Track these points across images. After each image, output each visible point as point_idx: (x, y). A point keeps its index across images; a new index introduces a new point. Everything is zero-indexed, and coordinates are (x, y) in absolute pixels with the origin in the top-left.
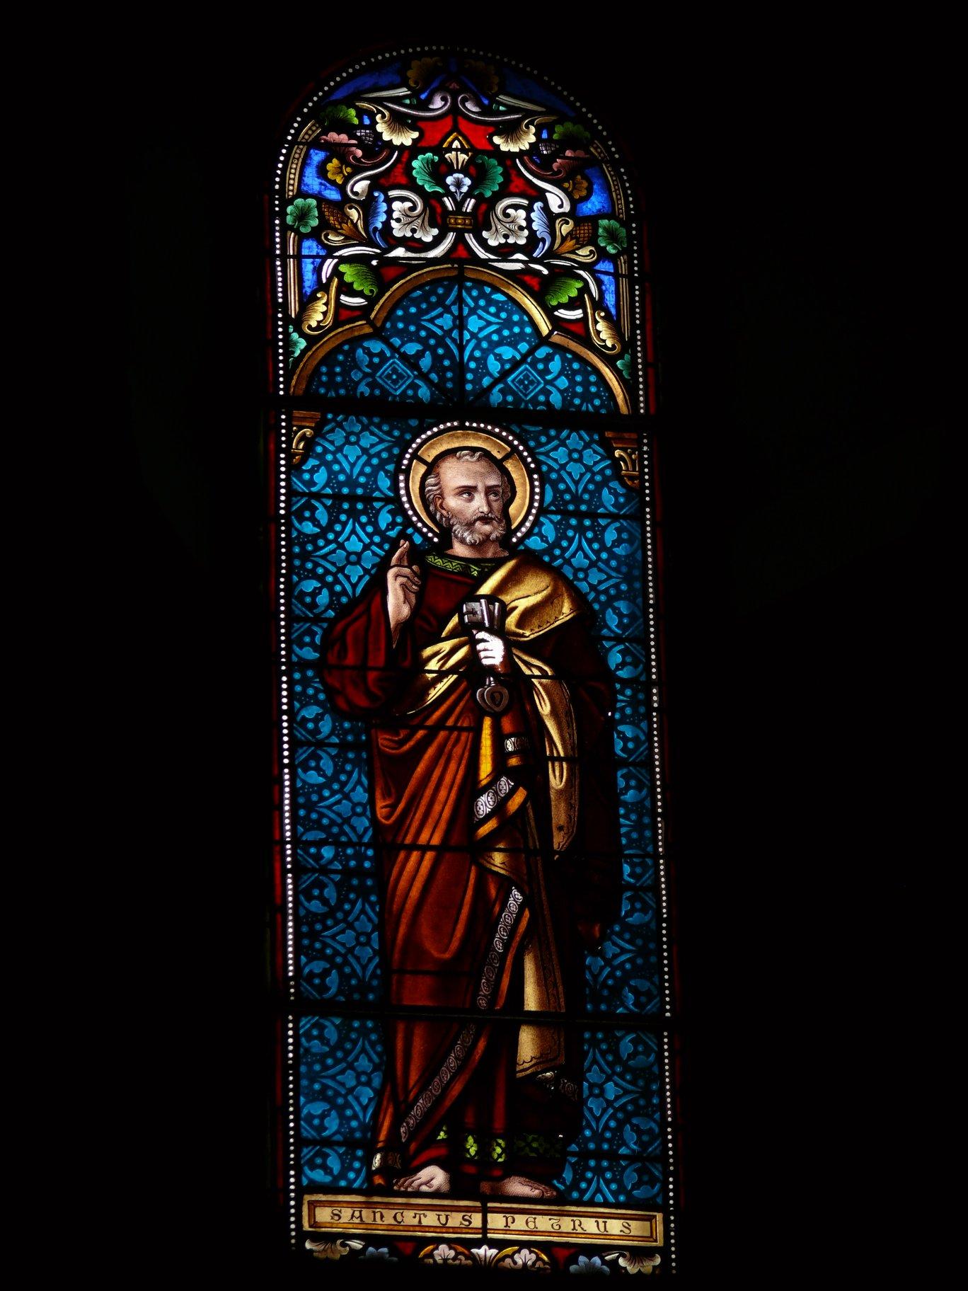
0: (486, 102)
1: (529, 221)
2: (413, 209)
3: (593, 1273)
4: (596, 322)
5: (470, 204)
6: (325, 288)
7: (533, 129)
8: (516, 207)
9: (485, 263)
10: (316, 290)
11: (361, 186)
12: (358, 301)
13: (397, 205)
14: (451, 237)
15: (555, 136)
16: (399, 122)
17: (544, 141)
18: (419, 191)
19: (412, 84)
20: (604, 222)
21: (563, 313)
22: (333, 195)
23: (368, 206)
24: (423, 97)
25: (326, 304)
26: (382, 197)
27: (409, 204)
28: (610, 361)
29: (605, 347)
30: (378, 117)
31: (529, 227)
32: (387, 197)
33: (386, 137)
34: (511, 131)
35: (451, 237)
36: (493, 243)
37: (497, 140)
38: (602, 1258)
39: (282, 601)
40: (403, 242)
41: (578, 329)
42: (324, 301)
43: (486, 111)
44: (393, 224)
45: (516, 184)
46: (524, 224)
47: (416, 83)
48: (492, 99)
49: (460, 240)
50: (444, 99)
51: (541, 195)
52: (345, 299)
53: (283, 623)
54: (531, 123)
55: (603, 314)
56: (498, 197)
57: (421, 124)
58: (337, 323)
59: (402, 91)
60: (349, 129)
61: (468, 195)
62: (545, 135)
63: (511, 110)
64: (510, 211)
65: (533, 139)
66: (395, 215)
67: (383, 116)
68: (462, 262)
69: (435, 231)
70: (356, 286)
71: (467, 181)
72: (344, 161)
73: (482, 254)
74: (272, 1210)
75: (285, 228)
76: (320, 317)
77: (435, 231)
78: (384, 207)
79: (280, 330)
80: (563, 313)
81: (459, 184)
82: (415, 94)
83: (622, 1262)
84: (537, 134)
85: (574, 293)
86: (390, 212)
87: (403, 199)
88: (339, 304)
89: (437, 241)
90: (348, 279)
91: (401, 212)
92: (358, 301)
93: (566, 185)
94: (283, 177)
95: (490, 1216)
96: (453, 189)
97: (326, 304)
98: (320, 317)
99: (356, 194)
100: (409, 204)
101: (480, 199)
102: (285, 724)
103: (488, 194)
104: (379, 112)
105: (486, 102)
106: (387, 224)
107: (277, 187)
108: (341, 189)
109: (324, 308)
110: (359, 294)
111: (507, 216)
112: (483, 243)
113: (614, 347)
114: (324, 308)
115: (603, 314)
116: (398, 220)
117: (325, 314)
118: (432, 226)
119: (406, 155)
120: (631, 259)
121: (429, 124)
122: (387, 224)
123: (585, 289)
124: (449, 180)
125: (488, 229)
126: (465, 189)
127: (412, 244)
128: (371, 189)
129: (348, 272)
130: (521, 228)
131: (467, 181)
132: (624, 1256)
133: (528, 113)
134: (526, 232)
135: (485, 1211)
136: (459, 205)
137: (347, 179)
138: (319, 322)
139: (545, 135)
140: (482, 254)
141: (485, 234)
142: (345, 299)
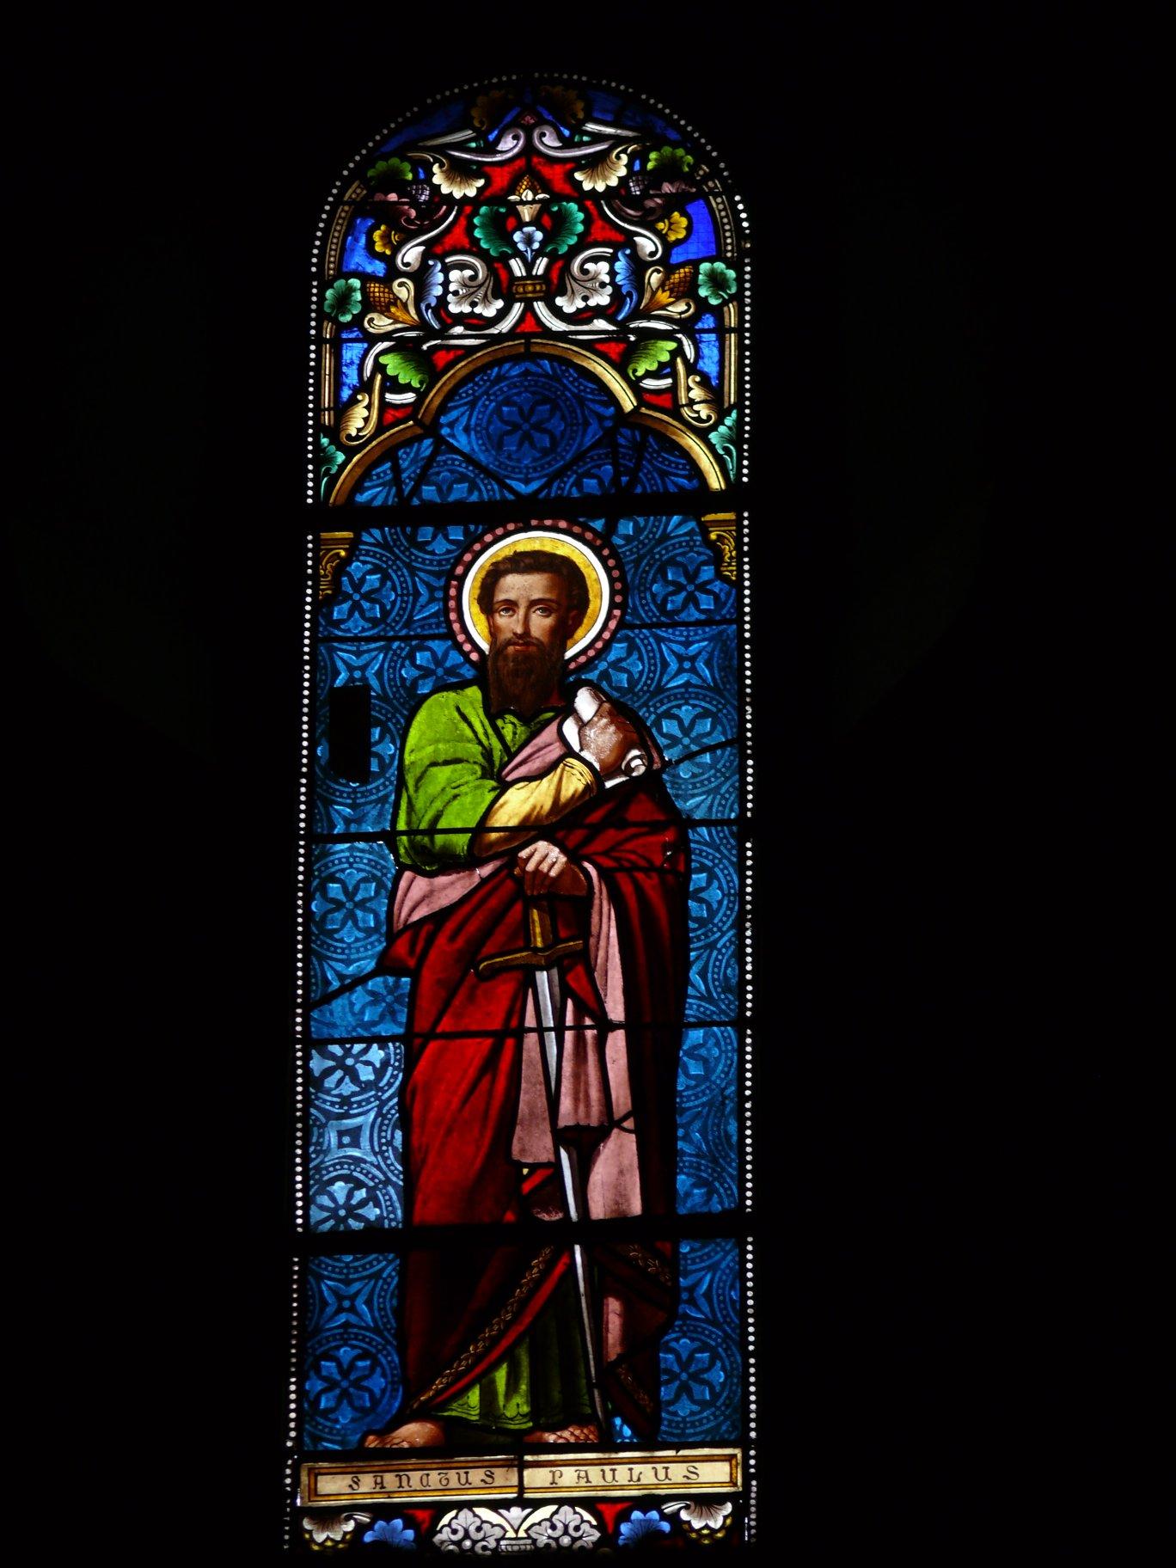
0: (567, 133)
1: (612, 273)
2: (473, 278)
3: (650, 1535)
4: (689, 389)
5: (541, 266)
6: (365, 386)
7: (624, 158)
8: (595, 259)
9: (562, 336)
10: (364, 391)
11: (411, 254)
12: (409, 397)
13: (455, 275)
14: (517, 308)
15: (650, 166)
16: (460, 171)
17: (636, 174)
18: (483, 255)
19: (477, 124)
20: (705, 267)
21: (650, 384)
22: (378, 268)
23: (420, 277)
24: (491, 137)
25: (368, 407)
26: (439, 266)
27: (468, 273)
28: (703, 434)
29: (699, 419)
30: (436, 168)
31: (613, 283)
32: (444, 264)
33: (445, 190)
34: (595, 164)
35: (517, 308)
36: (569, 309)
37: (578, 176)
38: (661, 1512)
39: (300, 965)
40: (460, 319)
41: (665, 401)
42: (366, 402)
43: (567, 144)
44: (450, 298)
45: (598, 232)
46: (607, 279)
47: (482, 123)
48: (577, 129)
49: (529, 310)
50: (516, 137)
51: (628, 240)
52: (391, 397)
53: (305, 761)
54: (624, 152)
55: (698, 379)
56: (575, 251)
57: (487, 169)
58: (381, 428)
59: (469, 133)
60: (402, 187)
61: (538, 253)
62: (637, 167)
63: (597, 138)
64: (587, 266)
65: (623, 172)
66: (452, 288)
67: (441, 166)
68: (528, 336)
69: (500, 304)
70: (402, 380)
71: (539, 236)
72: (393, 225)
73: (557, 325)
74: (275, 1512)
75: (322, 317)
76: (361, 424)
77: (500, 304)
78: (440, 277)
79: (300, 973)
80: (650, 384)
81: (529, 240)
82: (481, 135)
83: (684, 1515)
84: (629, 166)
85: (665, 357)
86: (446, 284)
87: (462, 266)
88: (384, 406)
89: (502, 314)
90: (390, 372)
91: (456, 282)
92: (409, 397)
93: (661, 226)
94: (321, 257)
95: (526, 1473)
96: (521, 247)
97: (368, 407)
98: (361, 424)
99: (407, 265)
100: (468, 273)
101: (553, 257)
102: (305, 727)
103: (563, 249)
104: (436, 160)
105: (567, 133)
106: (442, 301)
107: (313, 332)
108: (390, 261)
109: (365, 413)
110: (407, 388)
111: (586, 272)
112: (557, 312)
113: (709, 418)
114: (365, 413)
115: (698, 379)
116: (456, 293)
117: (366, 420)
118: (496, 298)
119: (468, 209)
120: (741, 306)
121: (498, 170)
122: (442, 301)
123: (679, 352)
124: (517, 237)
125: (563, 293)
126: (536, 246)
127: (474, 322)
128: (425, 257)
129: (392, 364)
130: (603, 285)
131: (539, 236)
132: (687, 1507)
133: (617, 141)
134: (609, 289)
135: (522, 1466)
136: (529, 266)
137: (396, 250)
138: (359, 430)
139: (637, 167)
140: (557, 325)
141: (559, 301)
142: (391, 397)
